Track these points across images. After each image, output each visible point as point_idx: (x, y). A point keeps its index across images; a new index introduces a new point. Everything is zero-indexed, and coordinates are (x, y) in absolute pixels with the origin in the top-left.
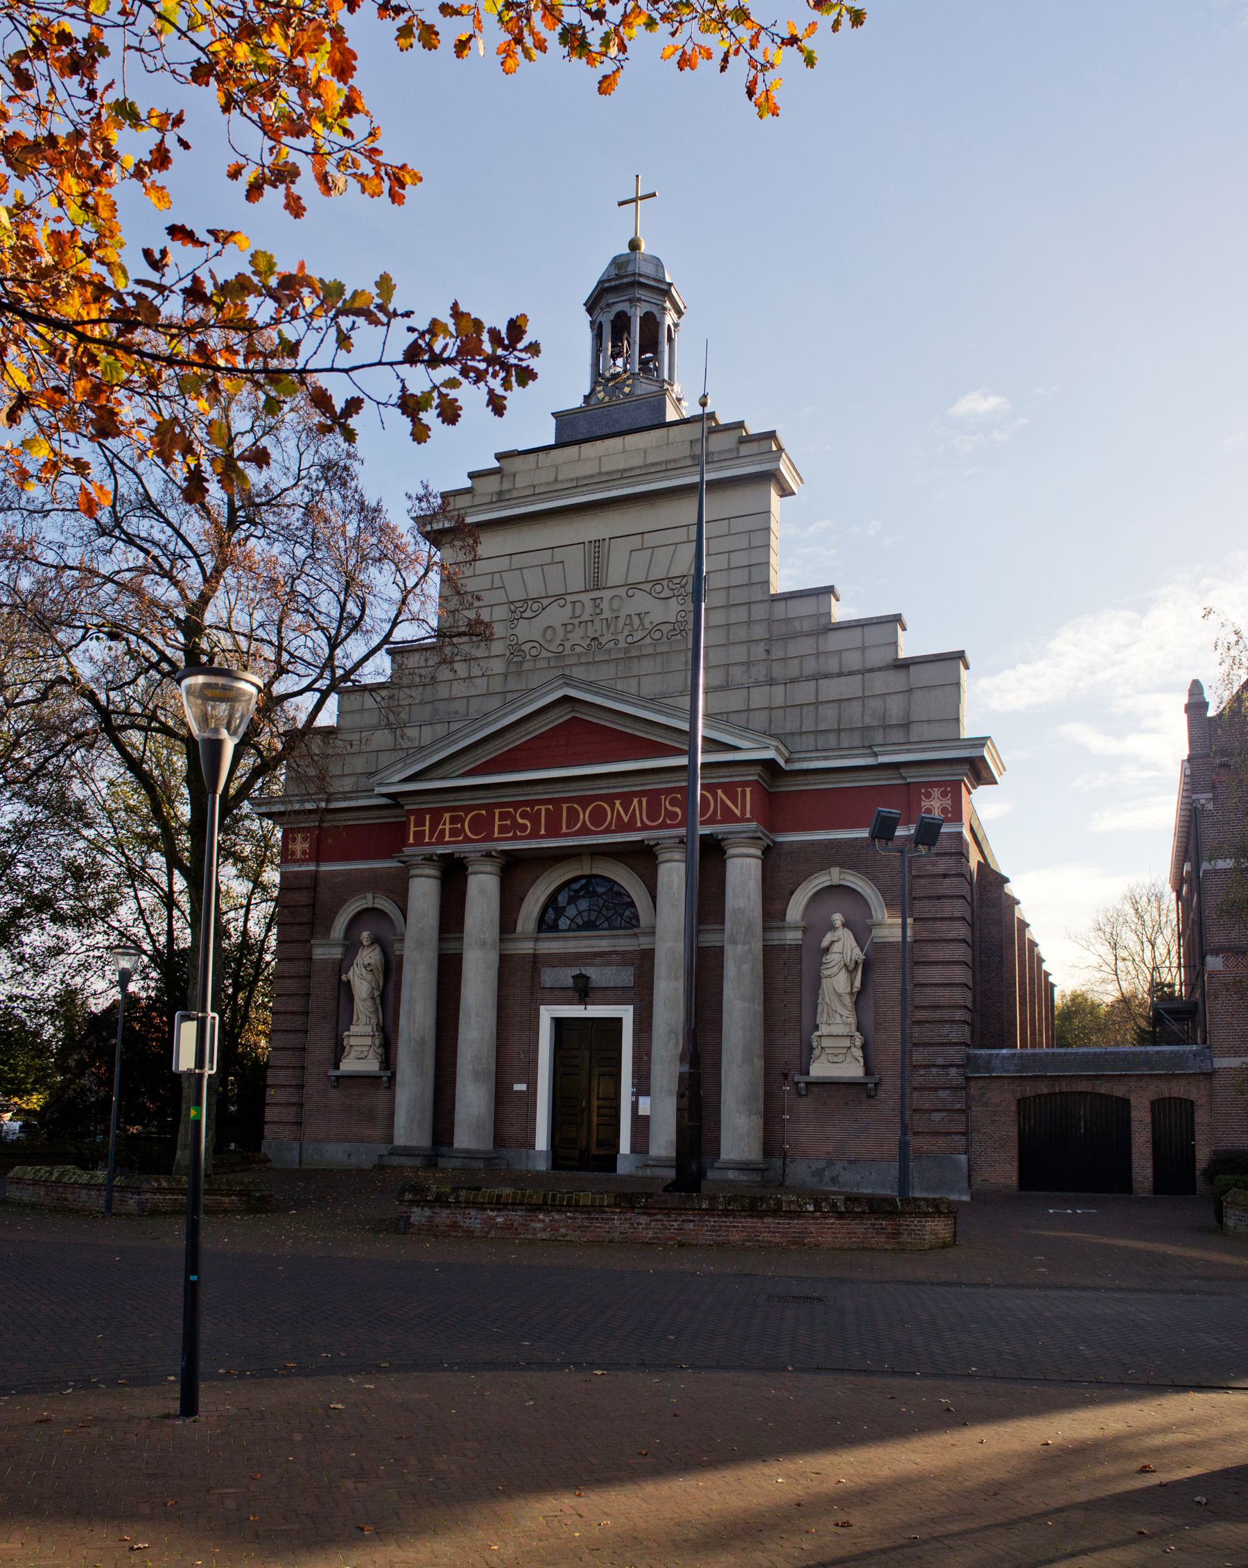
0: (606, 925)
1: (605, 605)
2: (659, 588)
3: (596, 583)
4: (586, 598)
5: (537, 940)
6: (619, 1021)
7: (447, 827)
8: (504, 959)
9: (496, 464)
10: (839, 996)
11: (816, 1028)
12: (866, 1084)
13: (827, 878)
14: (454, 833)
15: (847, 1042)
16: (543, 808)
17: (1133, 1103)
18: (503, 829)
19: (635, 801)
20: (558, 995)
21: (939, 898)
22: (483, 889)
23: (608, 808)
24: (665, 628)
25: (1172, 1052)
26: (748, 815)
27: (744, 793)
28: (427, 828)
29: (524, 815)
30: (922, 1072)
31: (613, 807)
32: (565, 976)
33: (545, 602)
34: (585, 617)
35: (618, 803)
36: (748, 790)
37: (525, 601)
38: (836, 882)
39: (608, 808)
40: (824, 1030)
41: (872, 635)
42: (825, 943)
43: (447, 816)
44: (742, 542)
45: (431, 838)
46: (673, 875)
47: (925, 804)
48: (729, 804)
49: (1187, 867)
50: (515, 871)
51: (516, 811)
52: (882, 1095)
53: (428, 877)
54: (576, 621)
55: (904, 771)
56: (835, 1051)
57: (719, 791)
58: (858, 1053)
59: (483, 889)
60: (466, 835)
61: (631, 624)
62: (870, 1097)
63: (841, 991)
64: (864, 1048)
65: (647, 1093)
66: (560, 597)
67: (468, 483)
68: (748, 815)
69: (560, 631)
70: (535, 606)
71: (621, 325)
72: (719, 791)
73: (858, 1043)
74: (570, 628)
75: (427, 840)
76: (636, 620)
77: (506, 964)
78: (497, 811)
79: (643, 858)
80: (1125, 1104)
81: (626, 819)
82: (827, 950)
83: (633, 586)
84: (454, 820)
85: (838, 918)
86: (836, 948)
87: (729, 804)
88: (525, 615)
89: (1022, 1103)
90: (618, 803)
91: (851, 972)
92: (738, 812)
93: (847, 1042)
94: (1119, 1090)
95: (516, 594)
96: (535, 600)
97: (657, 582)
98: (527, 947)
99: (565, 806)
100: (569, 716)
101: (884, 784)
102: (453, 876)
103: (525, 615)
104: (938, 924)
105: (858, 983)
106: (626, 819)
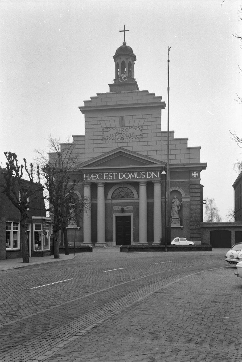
0: (127, 197)
1: (124, 130)
2: (136, 128)
3: (122, 125)
4: (120, 128)
5: (112, 200)
6: (117, 217)
7: (93, 177)
8: (106, 204)
9: (97, 96)
10: (176, 211)
11: (171, 217)
12: (181, 228)
13: (173, 189)
14: (94, 178)
15: (177, 220)
16: (115, 174)
17: (232, 232)
18: (106, 178)
19: (135, 173)
20: (117, 211)
21: (195, 193)
22: (101, 190)
23: (129, 175)
24: (138, 136)
25: (50, 241)
26: (159, 177)
27: (158, 173)
28: (88, 177)
29: (110, 175)
30: (192, 226)
31: (130, 174)
32: (119, 208)
33: (111, 128)
34: (120, 133)
35: (131, 173)
36: (159, 172)
37: (106, 128)
38: (175, 189)
39: (129, 175)
40: (173, 217)
41: (182, 142)
42: (173, 201)
43: (93, 174)
44: (155, 119)
45: (89, 179)
46: (143, 189)
47: (193, 175)
48: (155, 175)
49: (237, 198)
50: (107, 186)
51: (109, 174)
52: (184, 229)
53: (144, 185)
54: (118, 133)
55: (189, 168)
56: (175, 221)
57: (153, 172)
58: (179, 222)
59: (101, 190)
60: (97, 179)
61: (130, 135)
62: (181, 230)
63: (176, 210)
64: (180, 221)
65: (8, 239)
66: (114, 128)
67: (90, 99)
68: (159, 177)
69: (114, 135)
70: (108, 129)
71: (123, 63)
72: (153, 172)
73: (179, 220)
74: (116, 134)
75: (88, 179)
76: (131, 134)
77: (106, 204)
78: (104, 174)
79: (136, 185)
80: (230, 232)
81: (133, 177)
82: (173, 203)
83: (131, 127)
84: (94, 175)
85: (175, 196)
86: (175, 202)
87: (155, 175)
88: (106, 131)
89: (211, 232)
90: (131, 173)
91: (178, 207)
92: (157, 176)
93: (177, 220)
94: (229, 230)
95: (104, 126)
96: (109, 128)
97: (136, 126)
98: (110, 201)
99: (147, 172)
100: (120, 155)
101: (186, 171)
102: (94, 187)
103: (106, 131)
104: (195, 198)
105: (179, 209)
106: (133, 177)
